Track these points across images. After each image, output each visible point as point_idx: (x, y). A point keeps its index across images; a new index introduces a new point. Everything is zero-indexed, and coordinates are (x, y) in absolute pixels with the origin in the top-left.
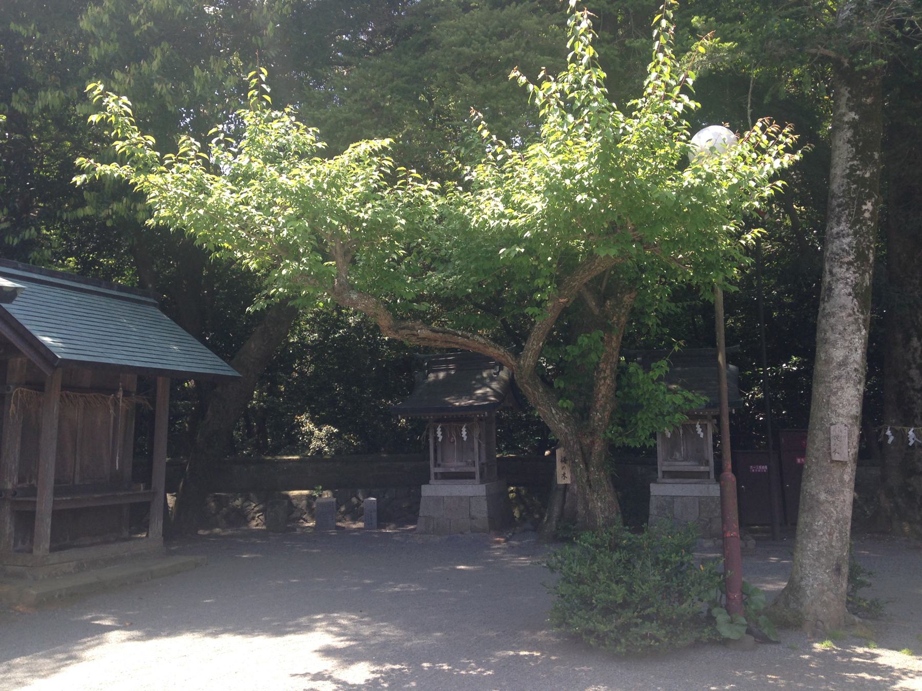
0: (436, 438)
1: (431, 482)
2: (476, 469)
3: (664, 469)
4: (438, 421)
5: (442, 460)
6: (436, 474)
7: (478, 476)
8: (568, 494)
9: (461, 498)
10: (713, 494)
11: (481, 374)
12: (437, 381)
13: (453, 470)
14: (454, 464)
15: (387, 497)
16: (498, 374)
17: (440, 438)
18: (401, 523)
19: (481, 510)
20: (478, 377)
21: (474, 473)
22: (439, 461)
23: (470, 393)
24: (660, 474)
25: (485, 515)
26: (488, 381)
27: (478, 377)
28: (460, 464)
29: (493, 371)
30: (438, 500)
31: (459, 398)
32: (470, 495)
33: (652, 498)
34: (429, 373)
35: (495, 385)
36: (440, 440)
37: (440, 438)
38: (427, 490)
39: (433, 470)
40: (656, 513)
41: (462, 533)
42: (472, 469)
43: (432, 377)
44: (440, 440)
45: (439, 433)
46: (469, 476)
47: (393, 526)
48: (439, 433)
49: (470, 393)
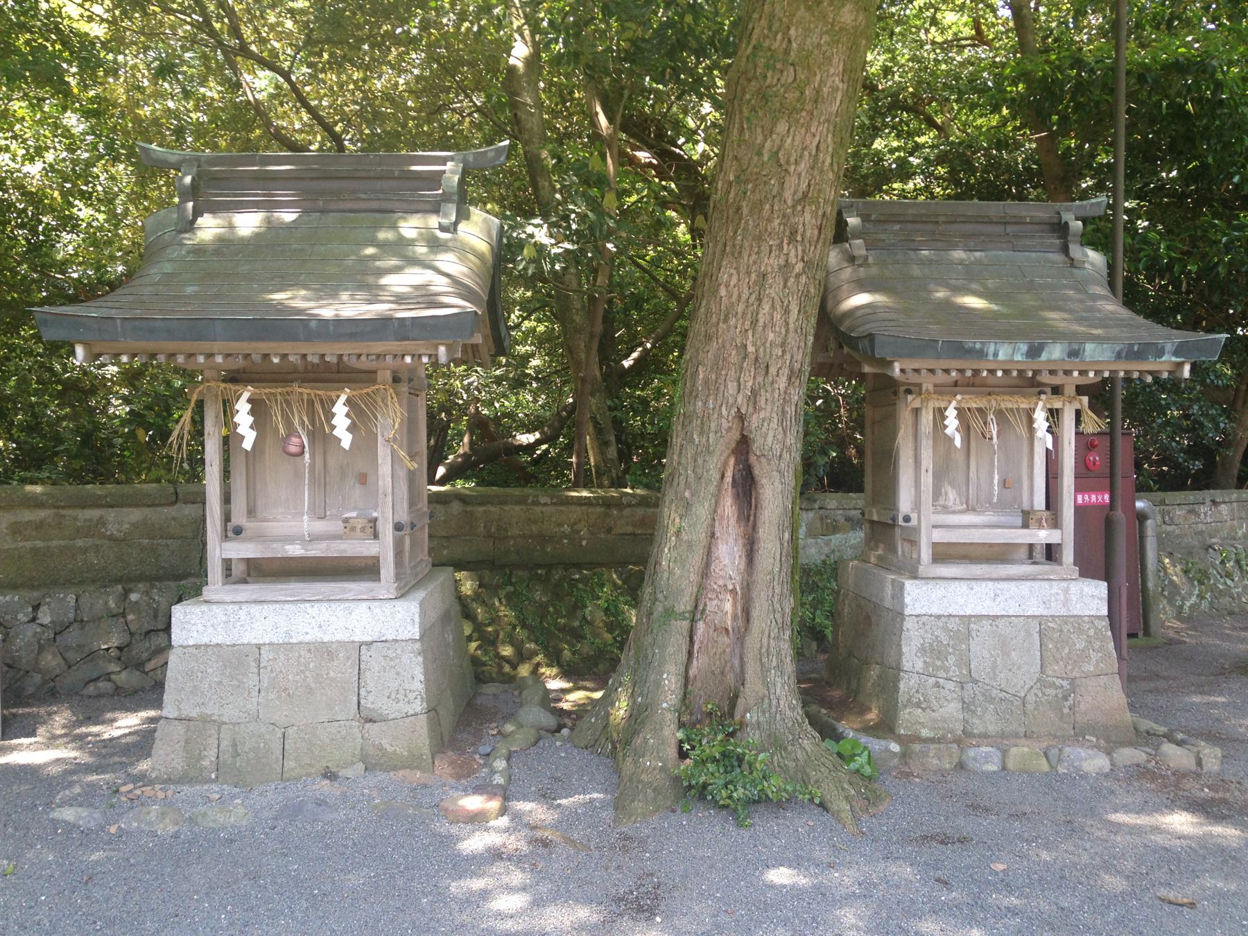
0: (229, 442)
1: (208, 593)
2: (383, 548)
3: (939, 536)
4: (236, 378)
5: (251, 512)
6: (227, 564)
7: (388, 569)
8: (701, 626)
9: (324, 651)
10: (1077, 609)
11: (394, 227)
12: (226, 245)
13: (295, 550)
14: (294, 527)
15: (45, 617)
16: (453, 228)
17: (249, 438)
18: (94, 701)
19: (404, 690)
20: (383, 235)
21: (376, 560)
22: (239, 518)
23: (365, 280)
24: (926, 554)
25: (419, 706)
26: (421, 250)
27: (383, 235)
28: (320, 526)
29: (434, 221)
30: (238, 660)
31: (329, 288)
32: (359, 637)
33: (909, 624)
34: (198, 213)
35: (450, 263)
36: (248, 444)
37: (249, 438)
38: (192, 624)
39: (218, 550)
40: (919, 665)
41: (330, 775)
42: (367, 548)
43: (209, 228)
44: (248, 444)
45: (243, 418)
46: (365, 570)
47: (61, 719)
48: (243, 418)
49: (365, 280)
